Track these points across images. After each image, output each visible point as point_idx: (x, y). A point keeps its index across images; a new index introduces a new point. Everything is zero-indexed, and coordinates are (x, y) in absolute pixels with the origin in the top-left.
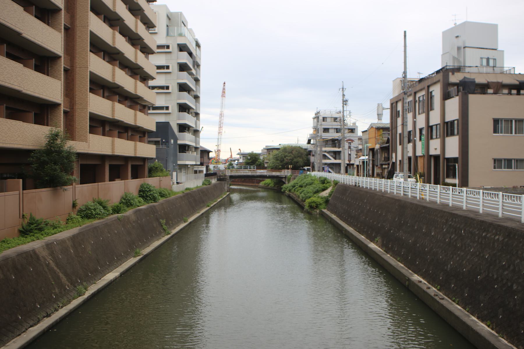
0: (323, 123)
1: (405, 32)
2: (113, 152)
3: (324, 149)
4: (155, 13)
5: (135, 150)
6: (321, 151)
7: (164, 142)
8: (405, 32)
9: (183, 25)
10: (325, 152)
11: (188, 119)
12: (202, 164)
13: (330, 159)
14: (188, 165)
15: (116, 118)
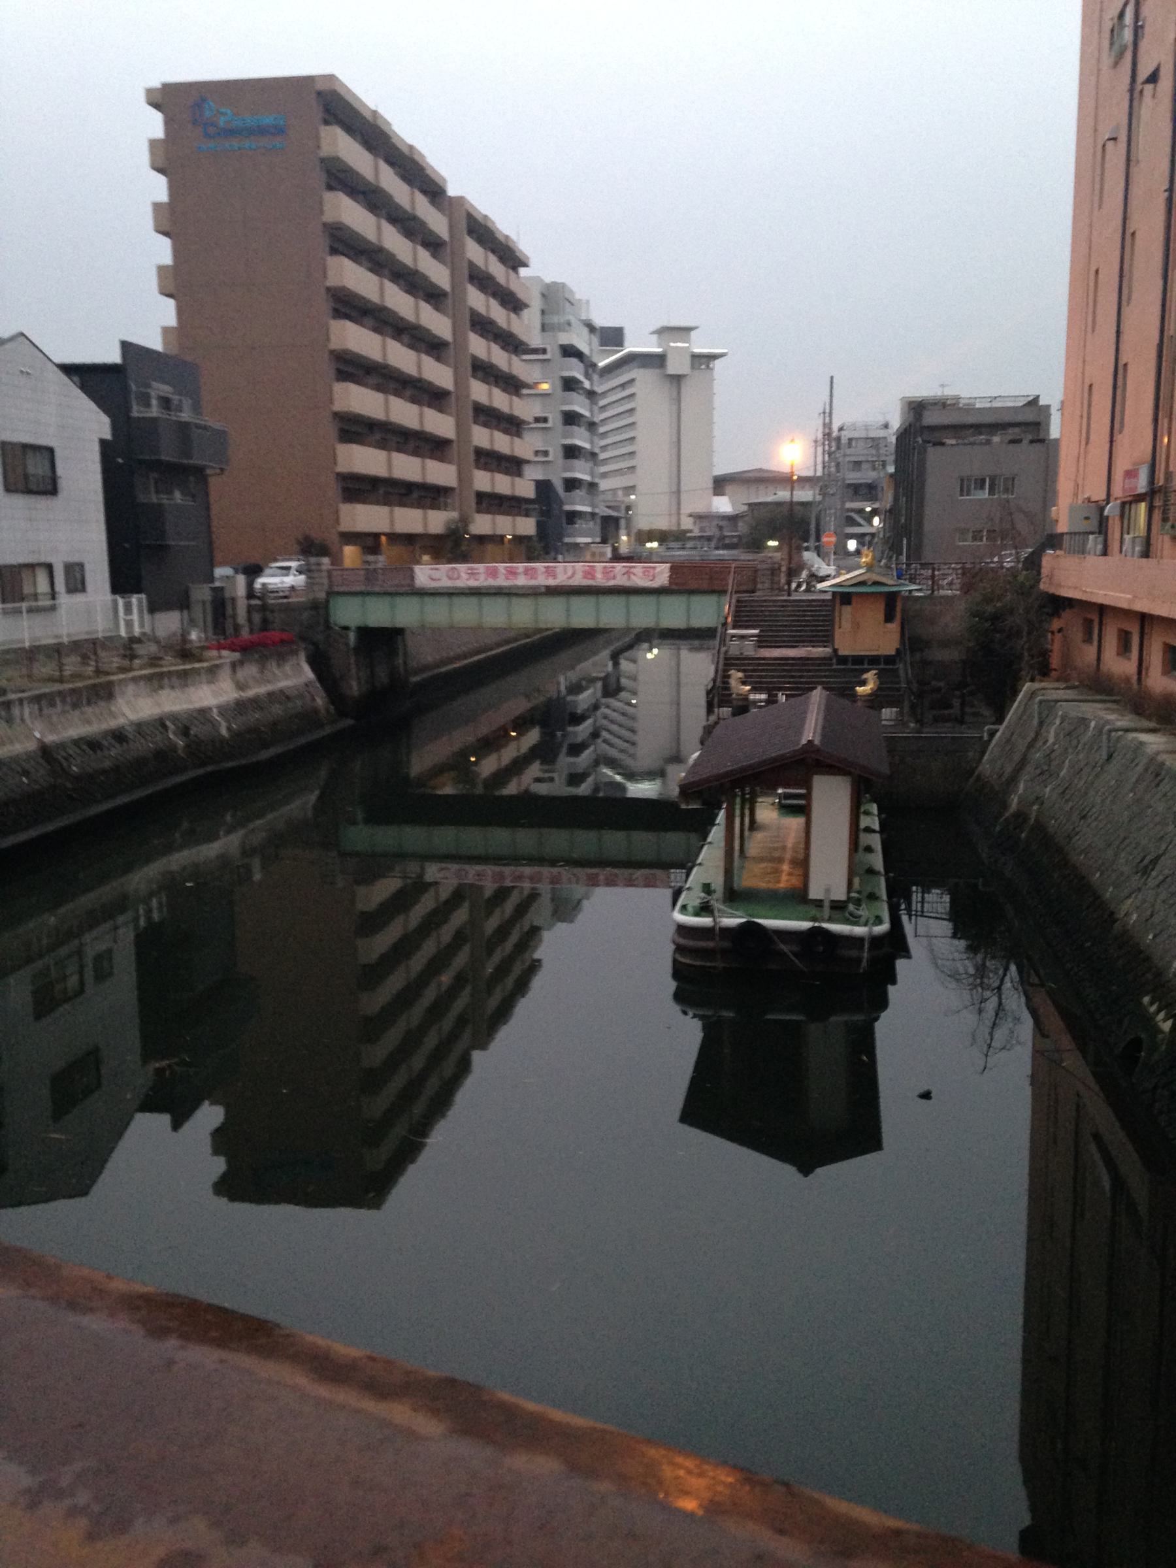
0: (848, 451)
1: (832, 377)
2: (391, 513)
3: (849, 505)
4: (759, 1557)
5: (494, 523)
6: (842, 508)
7: (747, 799)
8: (832, 377)
9: (568, 304)
10: (852, 510)
11: (581, 471)
12: (604, 541)
13: (860, 525)
14: (579, 544)
15: (496, 491)
